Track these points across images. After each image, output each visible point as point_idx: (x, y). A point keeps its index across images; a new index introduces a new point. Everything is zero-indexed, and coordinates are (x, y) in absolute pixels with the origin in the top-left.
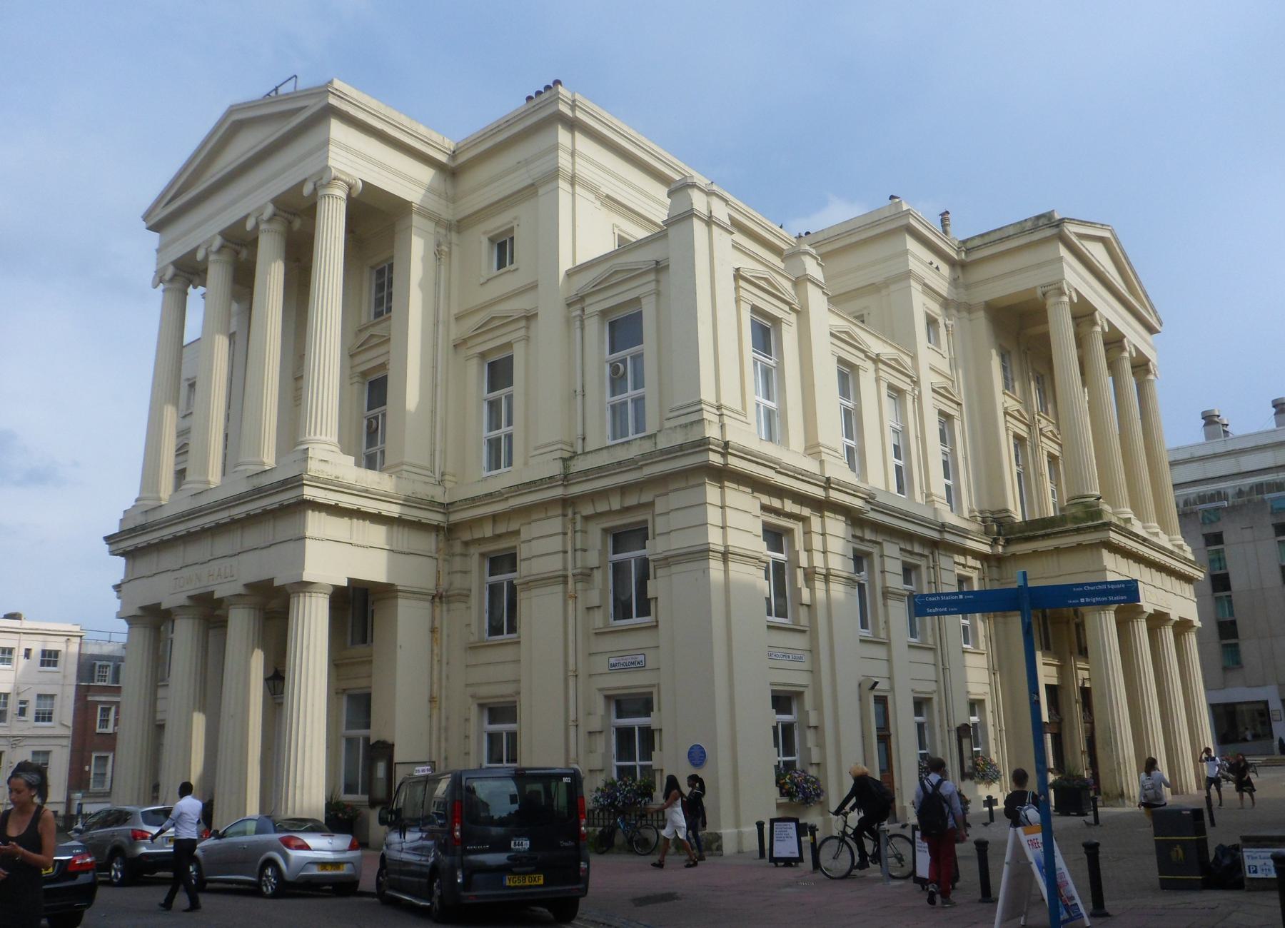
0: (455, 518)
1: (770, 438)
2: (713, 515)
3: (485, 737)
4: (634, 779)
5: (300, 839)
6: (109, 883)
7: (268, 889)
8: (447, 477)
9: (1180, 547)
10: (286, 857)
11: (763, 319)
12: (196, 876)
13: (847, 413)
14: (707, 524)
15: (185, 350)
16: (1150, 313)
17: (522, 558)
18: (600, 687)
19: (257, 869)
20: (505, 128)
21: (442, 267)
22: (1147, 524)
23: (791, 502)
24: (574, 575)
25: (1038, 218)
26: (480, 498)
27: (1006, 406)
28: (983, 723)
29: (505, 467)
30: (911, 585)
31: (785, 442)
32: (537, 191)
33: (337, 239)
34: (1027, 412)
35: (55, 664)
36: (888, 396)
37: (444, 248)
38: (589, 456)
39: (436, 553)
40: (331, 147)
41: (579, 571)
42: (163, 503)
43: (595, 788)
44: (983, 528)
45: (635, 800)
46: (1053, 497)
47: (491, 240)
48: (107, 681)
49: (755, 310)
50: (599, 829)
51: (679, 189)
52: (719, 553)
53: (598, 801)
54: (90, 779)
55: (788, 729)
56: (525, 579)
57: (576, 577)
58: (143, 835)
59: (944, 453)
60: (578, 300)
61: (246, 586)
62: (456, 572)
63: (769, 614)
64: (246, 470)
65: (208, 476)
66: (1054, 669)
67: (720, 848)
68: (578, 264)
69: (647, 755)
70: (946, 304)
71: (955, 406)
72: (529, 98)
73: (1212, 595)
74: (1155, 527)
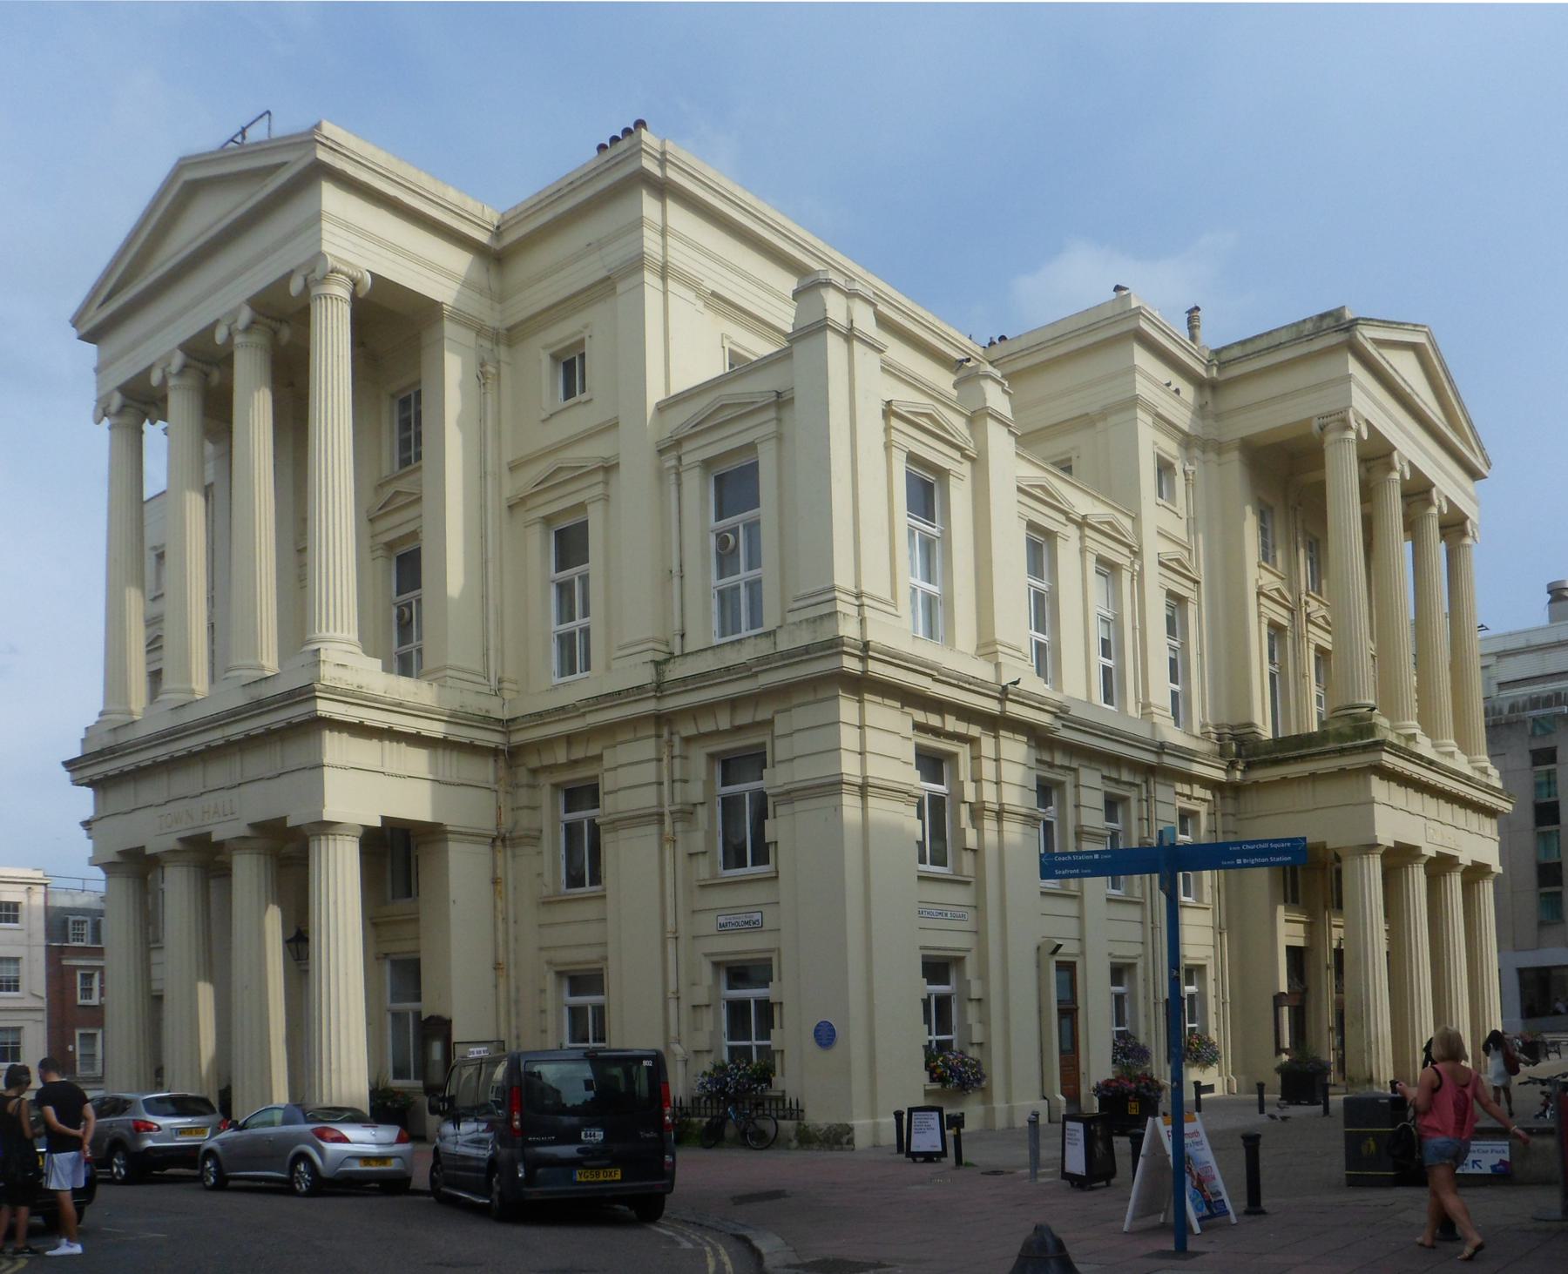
0: (518, 738)
1: (931, 633)
2: (849, 738)
3: (566, 1012)
4: (750, 1061)
5: (334, 1130)
6: (112, 1181)
7: (301, 1187)
8: (506, 685)
9: (1484, 771)
10: (321, 1151)
11: (923, 470)
12: (215, 1172)
13: (1039, 597)
14: (840, 748)
15: (147, 508)
16: (1474, 451)
17: (606, 790)
18: (707, 951)
19: (287, 1164)
20: (569, 192)
21: (489, 395)
22: (1440, 741)
23: (954, 718)
24: (672, 813)
25: (1322, 317)
26: (548, 713)
27: (1260, 583)
28: (1202, 994)
29: (581, 672)
30: (1117, 822)
31: (949, 641)
32: (615, 288)
33: (340, 359)
34: (1290, 591)
35: (15, 919)
36: (1097, 572)
37: (490, 369)
38: (690, 659)
39: (495, 783)
40: (325, 225)
41: (678, 807)
42: (136, 718)
43: (702, 1072)
44: (1217, 748)
45: (750, 1085)
46: (1319, 703)
47: (555, 357)
48: (85, 940)
49: (912, 458)
50: (708, 1119)
51: (810, 286)
52: (856, 786)
53: (704, 1087)
54: (75, 1061)
55: (943, 1003)
56: (609, 818)
57: (675, 815)
58: (148, 1127)
59: (1172, 649)
60: (672, 446)
61: (253, 826)
62: (521, 808)
63: (922, 861)
64: (239, 676)
65: (191, 682)
66: (1301, 926)
67: (851, 1141)
68: (672, 394)
69: (764, 1033)
70: (1187, 442)
71: (1190, 585)
72: (602, 147)
73: (1534, 830)
74: (1450, 744)
